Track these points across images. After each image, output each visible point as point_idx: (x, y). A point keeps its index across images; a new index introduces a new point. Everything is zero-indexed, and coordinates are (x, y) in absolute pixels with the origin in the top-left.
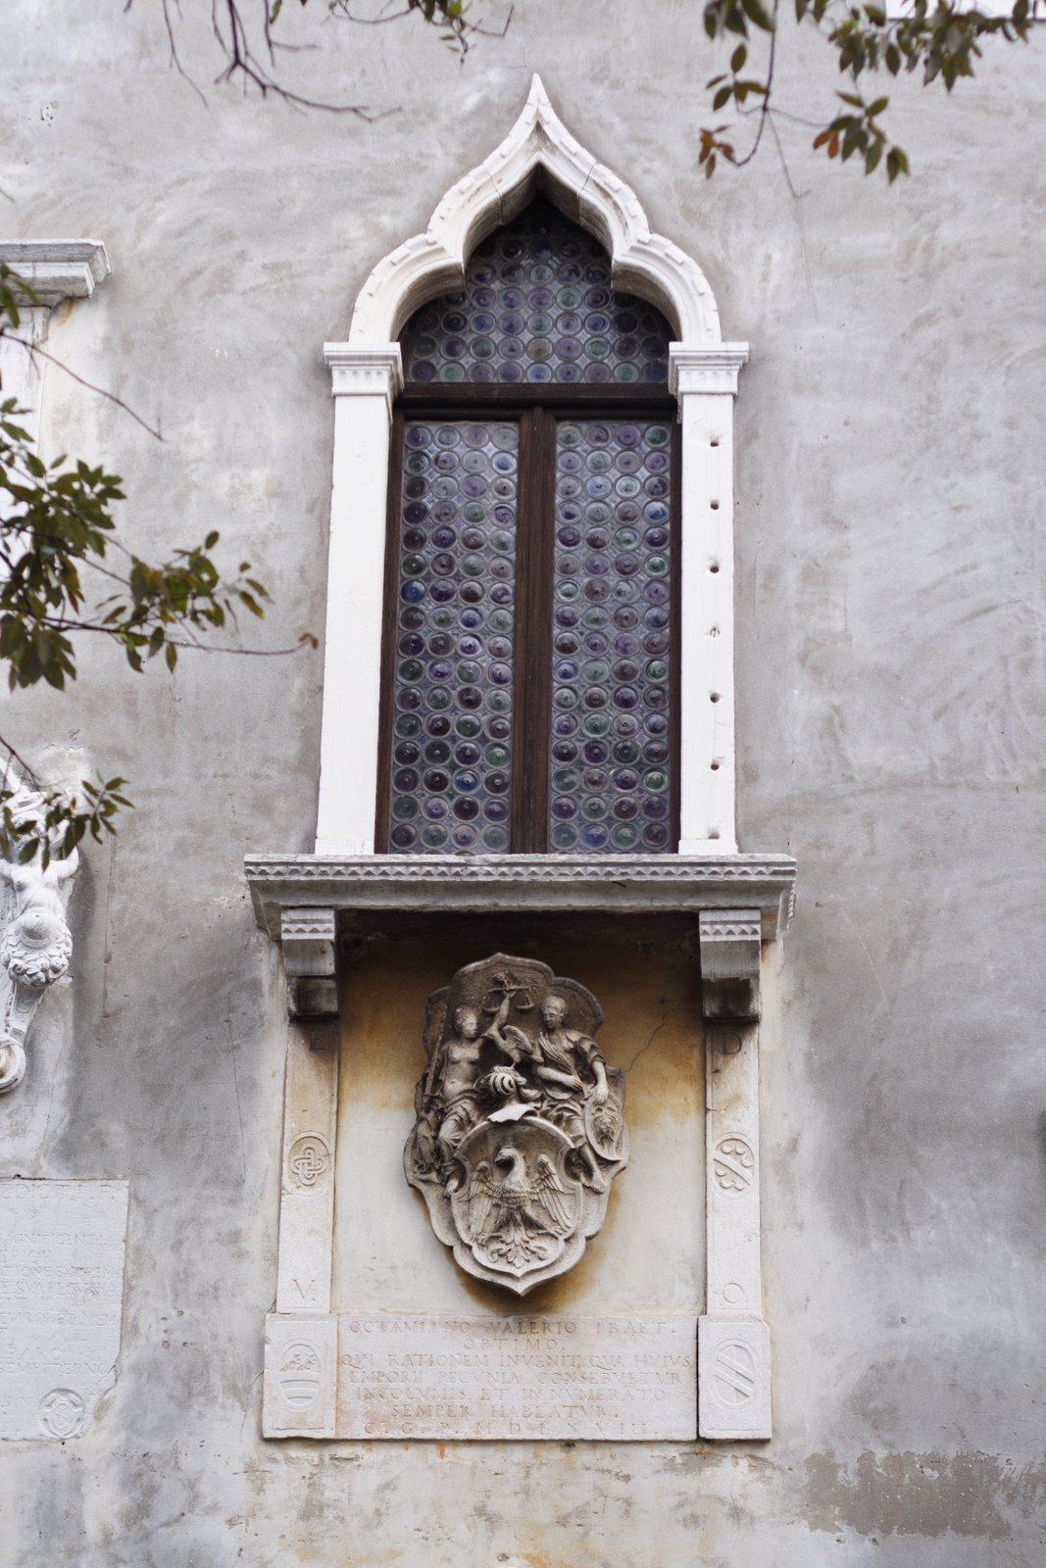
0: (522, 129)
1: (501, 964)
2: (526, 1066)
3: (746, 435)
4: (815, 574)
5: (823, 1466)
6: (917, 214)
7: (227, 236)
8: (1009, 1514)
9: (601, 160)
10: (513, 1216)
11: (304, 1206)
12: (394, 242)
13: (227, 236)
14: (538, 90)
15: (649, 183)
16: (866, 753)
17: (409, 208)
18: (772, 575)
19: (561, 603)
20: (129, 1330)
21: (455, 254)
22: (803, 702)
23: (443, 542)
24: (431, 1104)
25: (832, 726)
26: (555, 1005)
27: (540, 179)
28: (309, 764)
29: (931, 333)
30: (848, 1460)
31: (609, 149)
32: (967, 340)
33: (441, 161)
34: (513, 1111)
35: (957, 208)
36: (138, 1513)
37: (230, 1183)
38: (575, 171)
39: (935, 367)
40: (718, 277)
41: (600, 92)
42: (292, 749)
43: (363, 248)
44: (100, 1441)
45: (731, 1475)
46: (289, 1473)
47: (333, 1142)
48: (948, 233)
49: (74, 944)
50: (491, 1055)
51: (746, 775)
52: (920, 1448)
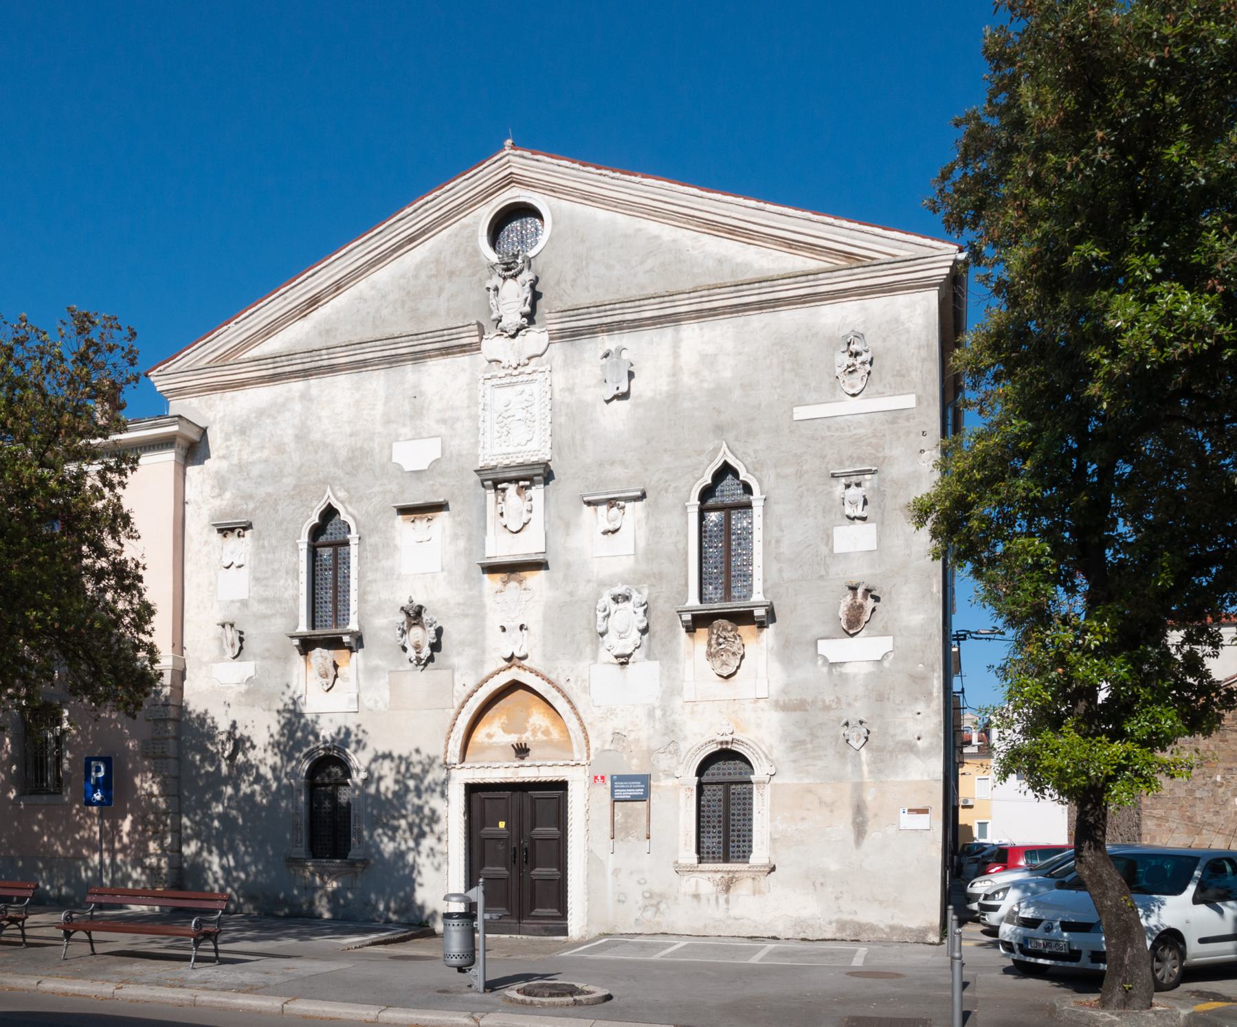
0: (721, 454)
1: (720, 621)
2: (725, 638)
3: (765, 514)
4: (778, 541)
5: (777, 702)
6: (799, 464)
7: (666, 481)
8: (808, 708)
9: (737, 458)
10: (724, 663)
12: (698, 479)
13: (666, 481)
14: (724, 445)
15: (746, 462)
16: (787, 575)
17: (700, 472)
18: (770, 542)
19: (733, 547)
20: (661, 685)
21: (709, 481)
22: (775, 567)
23: (711, 536)
24: (710, 645)
25: (781, 570)
26: (729, 628)
27: (726, 463)
28: (686, 585)
29: (801, 489)
30: (781, 700)
31: (739, 456)
32: (808, 490)
33: (706, 462)
34: (723, 646)
35: (806, 461)
36: (664, 715)
37: (677, 661)
38: (733, 462)
39: (801, 497)
40: (760, 481)
41: (736, 443)
42: (684, 582)
43: (692, 481)
44: (657, 704)
45: (762, 703)
47: (667, 940)
48: (804, 467)
49: (504, 227)
50: (719, 636)
51: (765, 581)
52: (793, 698)
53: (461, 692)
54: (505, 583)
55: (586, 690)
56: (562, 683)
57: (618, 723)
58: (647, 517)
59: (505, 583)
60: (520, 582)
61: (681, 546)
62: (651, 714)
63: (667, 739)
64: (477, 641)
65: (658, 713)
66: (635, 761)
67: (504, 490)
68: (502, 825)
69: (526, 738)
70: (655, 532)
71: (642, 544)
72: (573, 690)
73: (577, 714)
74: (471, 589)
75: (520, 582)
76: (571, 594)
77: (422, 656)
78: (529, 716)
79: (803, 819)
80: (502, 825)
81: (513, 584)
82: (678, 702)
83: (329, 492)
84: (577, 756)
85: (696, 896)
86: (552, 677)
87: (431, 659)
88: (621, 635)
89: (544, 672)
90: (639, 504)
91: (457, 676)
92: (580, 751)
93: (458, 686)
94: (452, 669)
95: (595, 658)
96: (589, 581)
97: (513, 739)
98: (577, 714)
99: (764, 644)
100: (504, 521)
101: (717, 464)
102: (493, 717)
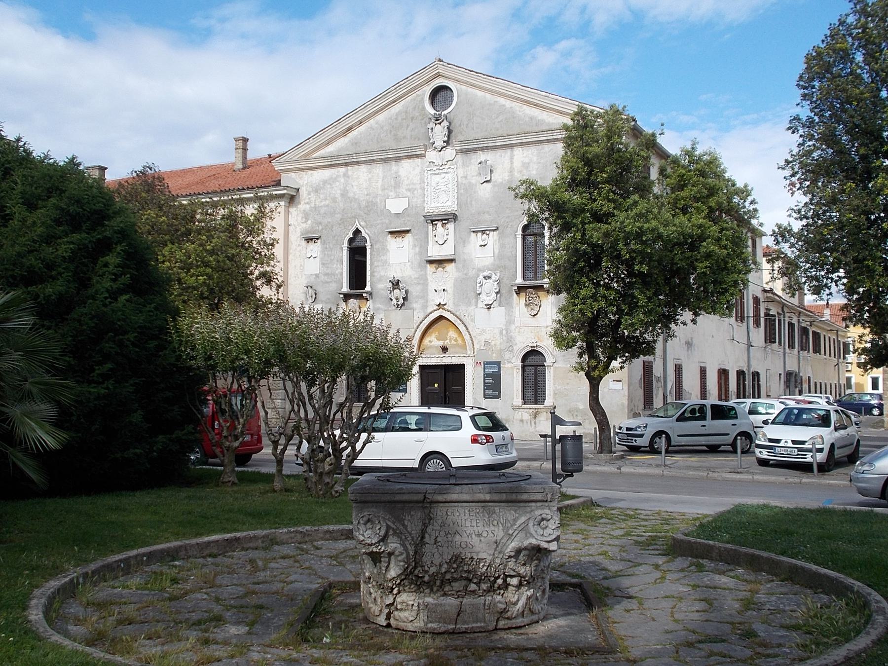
11: (517, 309)
27: (461, 368)
44: (504, 328)
46: (517, 329)
53: (417, 320)
54: (437, 269)
55: (473, 320)
56: (462, 317)
57: (486, 336)
58: (499, 239)
59: (437, 269)
60: (443, 268)
61: (513, 253)
62: (501, 333)
63: (508, 345)
64: (424, 296)
65: (504, 332)
66: (494, 355)
67: (436, 224)
68: (436, 385)
69: (447, 343)
70: (502, 246)
71: (497, 252)
72: (467, 320)
73: (469, 332)
74: (421, 271)
75: (443, 268)
76: (466, 274)
77: (399, 303)
78: (448, 332)
79: (568, 384)
80: (436, 385)
81: (440, 269)
82: (513, 327)
83: (357, 222)
84: (469, 352)
85: (522, 421)
86: (458, 314)
87: (403, 304)
88: (488, 294)
89: (454, 312)
90: (495, 233)
91: (415, 313)
92: (470, 350)
93: (416, 318)
94: (413, 309)
95: (476, 306)
96: (474, 269)
97: (441, 343)
98: (469, 332)
99: (550, 301)
100: (436, 239)
101: (354, 229)
102: (432, 332)
